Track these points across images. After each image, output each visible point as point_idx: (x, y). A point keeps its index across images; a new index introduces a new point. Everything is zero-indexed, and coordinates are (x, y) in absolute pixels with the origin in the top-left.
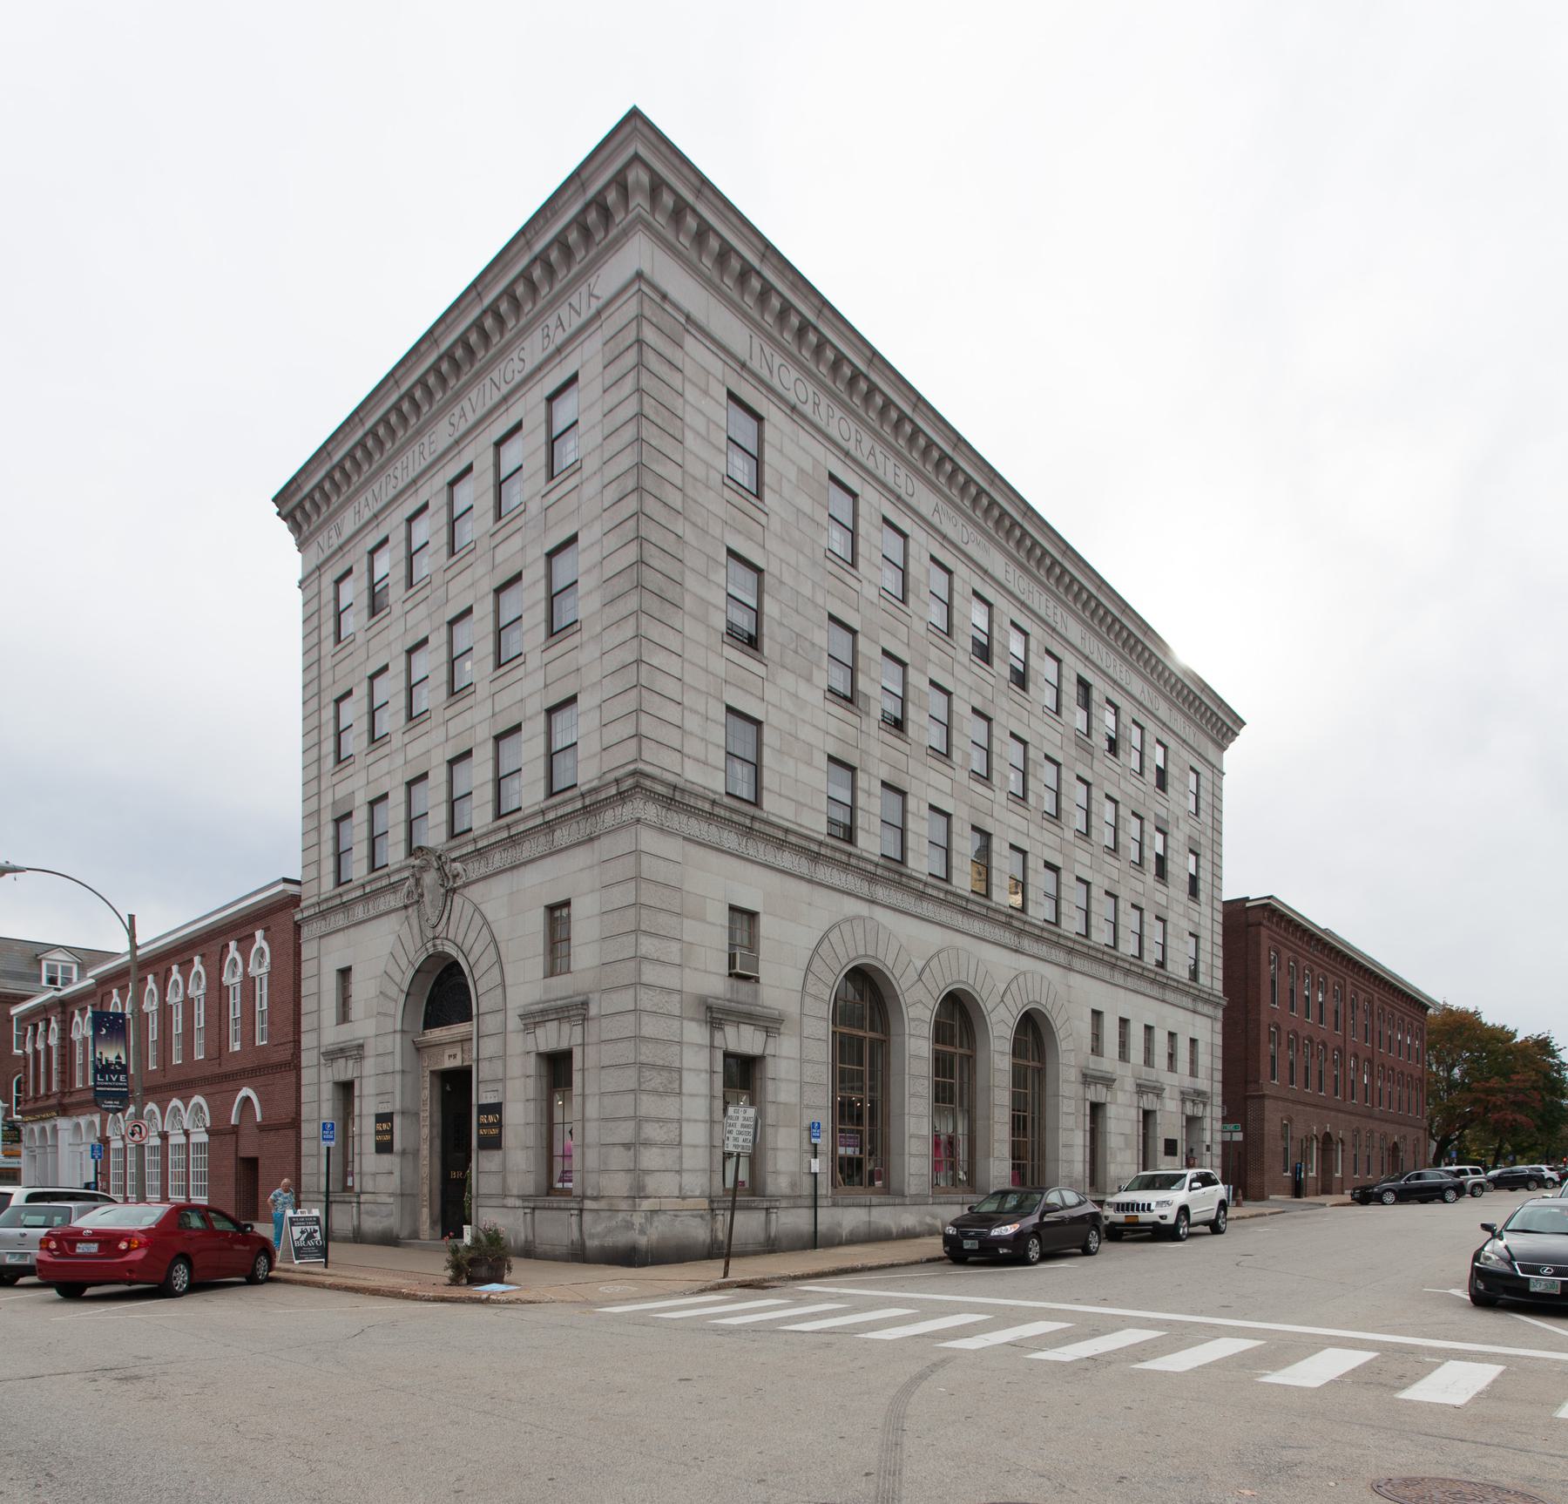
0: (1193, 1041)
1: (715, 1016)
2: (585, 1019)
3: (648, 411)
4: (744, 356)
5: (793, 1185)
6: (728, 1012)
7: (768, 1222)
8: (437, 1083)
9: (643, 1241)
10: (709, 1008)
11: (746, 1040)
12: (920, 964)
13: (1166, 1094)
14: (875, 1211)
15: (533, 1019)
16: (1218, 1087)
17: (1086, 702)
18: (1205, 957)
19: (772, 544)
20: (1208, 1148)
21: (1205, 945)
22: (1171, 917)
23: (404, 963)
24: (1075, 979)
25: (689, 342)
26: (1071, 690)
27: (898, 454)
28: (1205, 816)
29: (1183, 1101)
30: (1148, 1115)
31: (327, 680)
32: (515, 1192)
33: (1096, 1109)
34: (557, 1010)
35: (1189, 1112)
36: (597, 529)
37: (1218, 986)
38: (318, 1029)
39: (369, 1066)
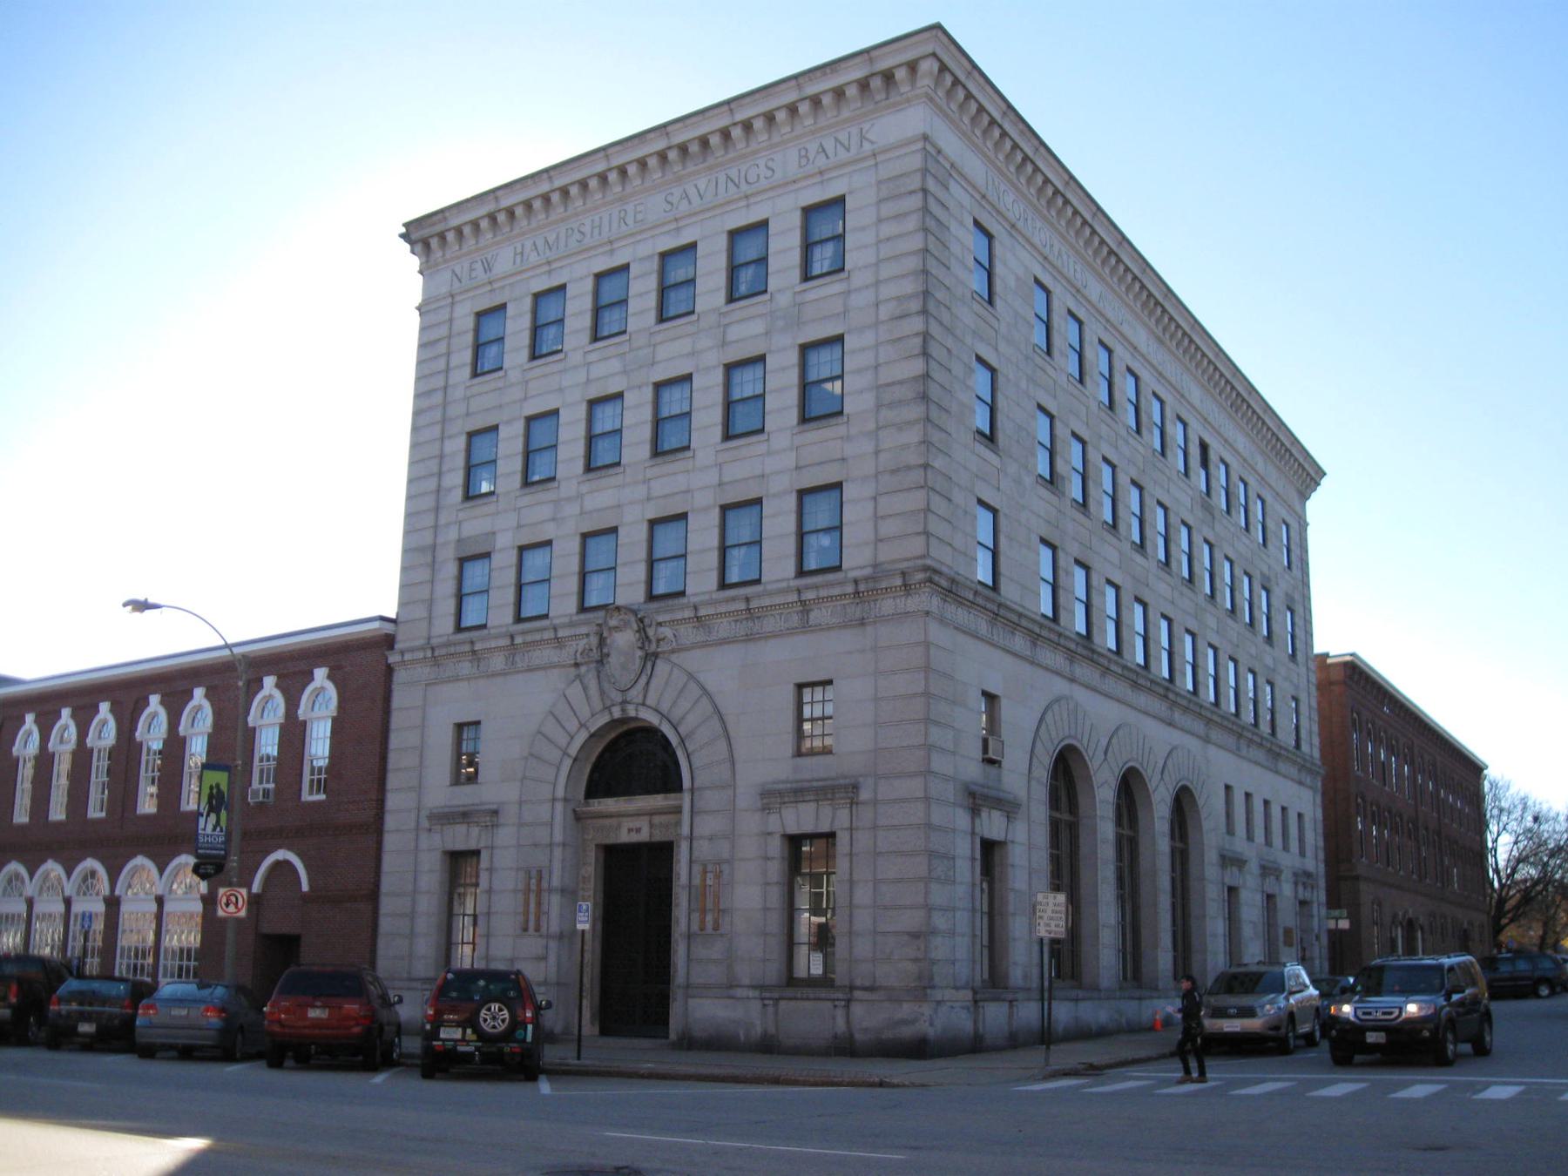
0: (1300, 816)
1: (977, 800)
2: (853, 803)
3: (931, 247)
4: (983, 191)
5: (1025, 977)
6: (986, 797)
7: (1011, 1016)
8: (601, 856)
9: (931, 1032)
10: (972, 795)
11: (993, 825)
12: (1104, 742)
13: (1283, 877)
14: (1082, 1005)
15: (772, 798)
16: (1322, 867)
17: (1205, 463)
18: (1304, 722)
19: (1002, 347)
20: (1318, 938)
21: (1304, 709)
22: (1279, 681)
23: (572, 725)
24: (1213, 751)
25: (953, 186)
26: (1195, 452)
27: (1077, 252)
28: (1296, 572)
29: (1296, 884)
30: (1270, 898)
31: (456, 410)
32: (746, 981)
33: (1232, 890)
34: (817, 790)
35: (1301, 897)
36: (869, 338)
37: (1316, 754)
38: (419, 789)
39: (505, 835)
